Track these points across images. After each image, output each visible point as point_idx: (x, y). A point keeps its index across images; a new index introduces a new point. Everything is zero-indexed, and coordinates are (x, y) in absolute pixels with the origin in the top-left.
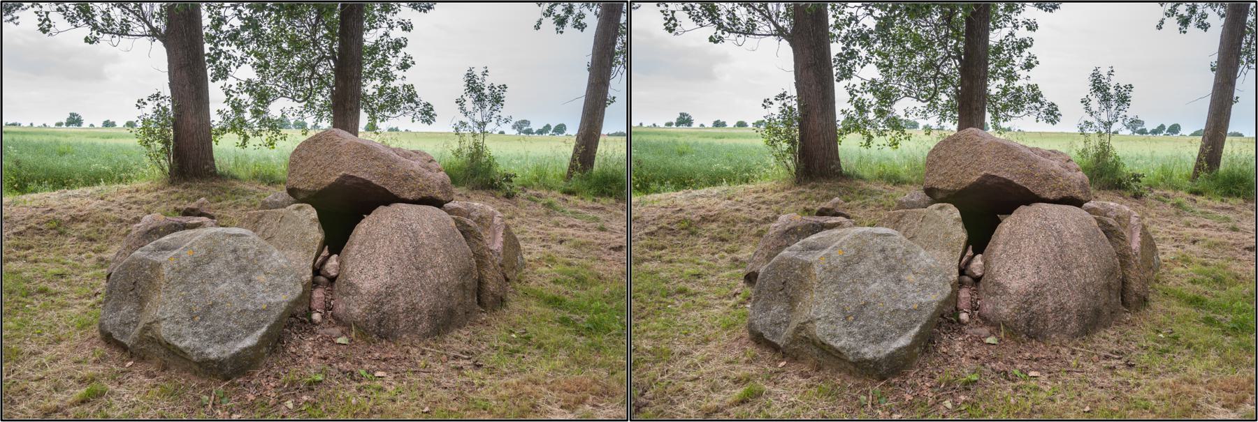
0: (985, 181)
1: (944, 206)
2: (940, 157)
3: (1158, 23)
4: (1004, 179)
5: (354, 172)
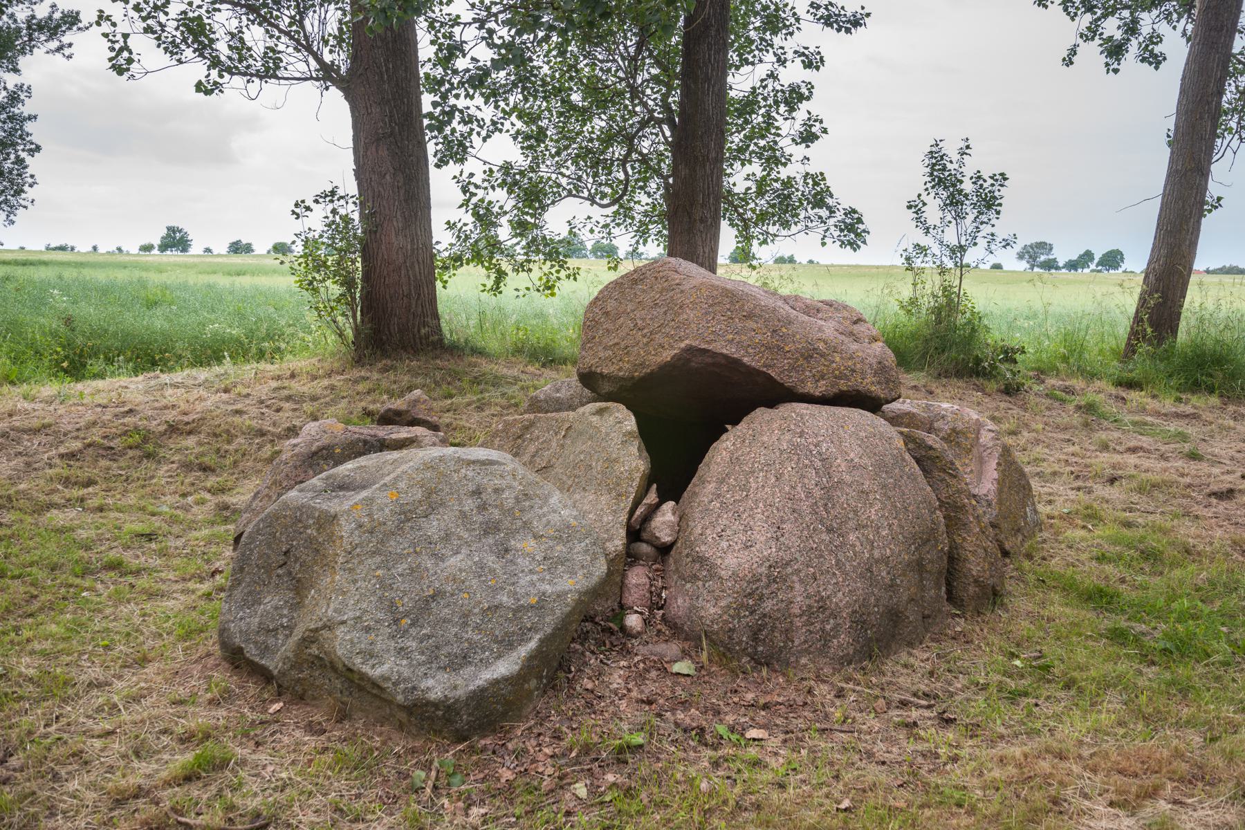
0: (689, 360)
1: (607, 408)
3: (1065, 54)
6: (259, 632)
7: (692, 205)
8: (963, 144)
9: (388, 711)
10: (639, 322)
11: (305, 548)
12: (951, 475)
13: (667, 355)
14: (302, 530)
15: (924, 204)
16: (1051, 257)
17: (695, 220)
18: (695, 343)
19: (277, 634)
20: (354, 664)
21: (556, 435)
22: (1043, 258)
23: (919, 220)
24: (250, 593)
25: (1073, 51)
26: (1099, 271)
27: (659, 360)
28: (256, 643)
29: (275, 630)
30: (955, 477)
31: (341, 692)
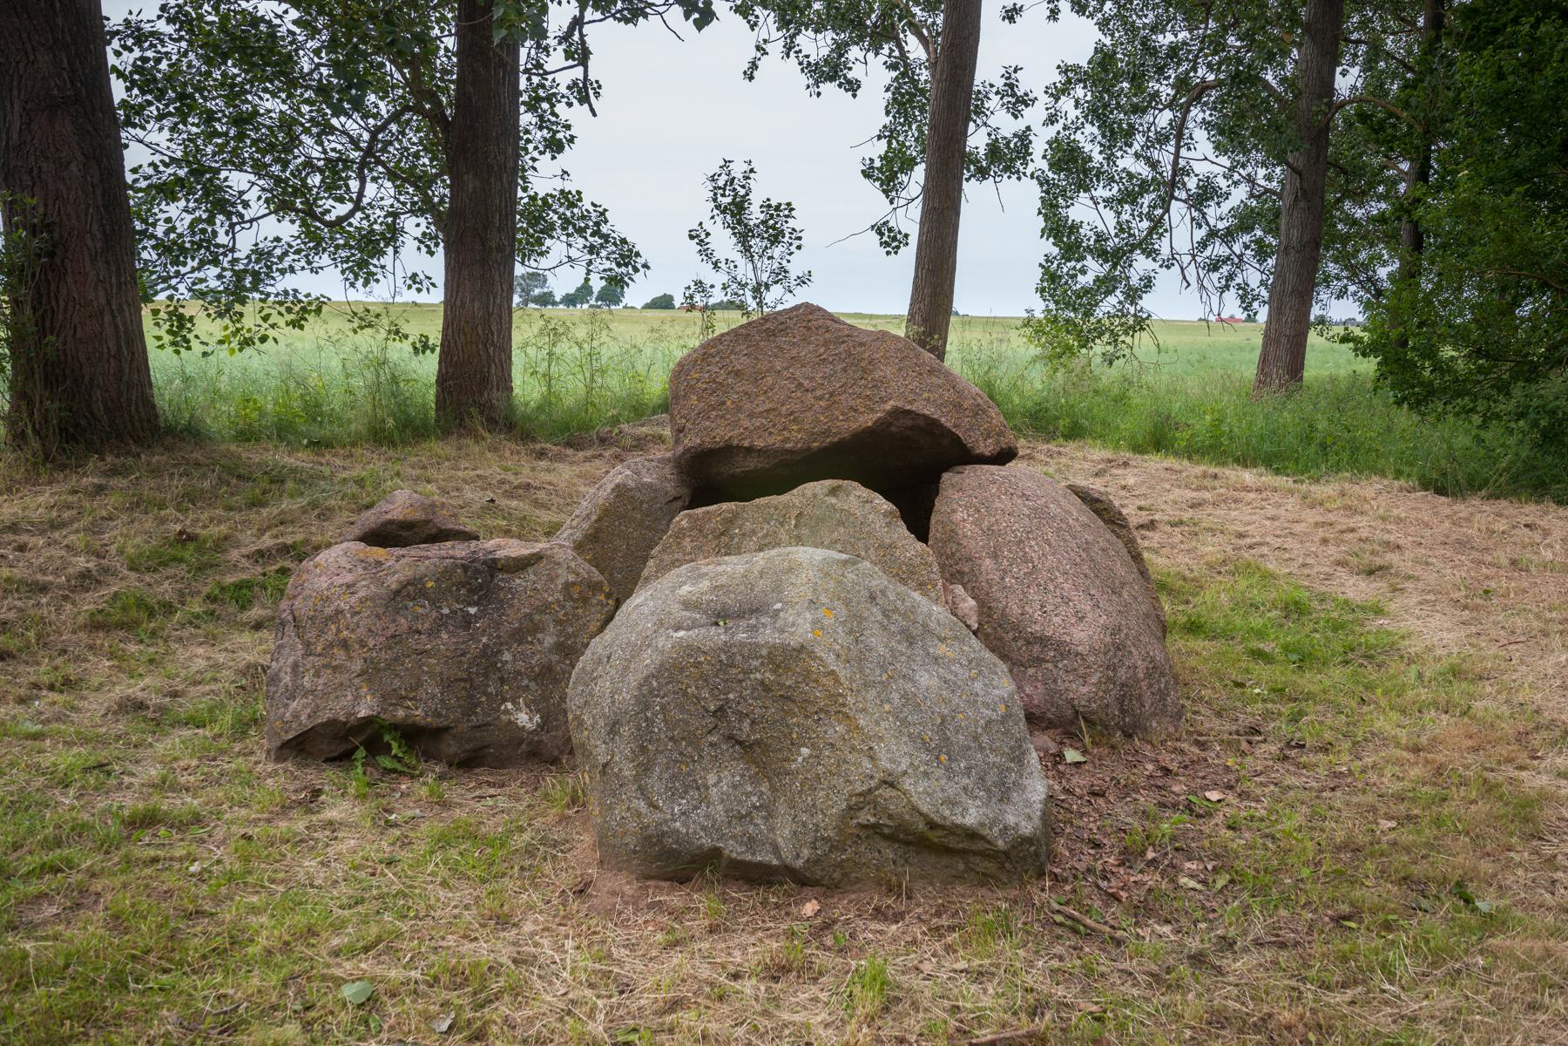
0: (890, 424)
1: (839, 487)
2: (737, 373)
3: (746, 66)
4: (925, 417)
5: (911, 402)
6: (729, 823)
7: (486, 229)
8: (746, 167)
9: (961, 867)
10: (806, 383)
11: (755, 699)
12: (1121, 526)
13: (868, 420)
14: (741, 676)
15: (708, 234)
16: (546, 290)
17: (491, 249)
18: (900, 404)
19: (751, 820)
20: (945, 818)
21: (782, 524)
22: (537, 291)
23: (706, 252)
24: (674, 777)
25: (754, 65)
26: (599, 307)
27: (854, 426)
28: (734, 837)
29: (749, 814)
30: (1124, 527)
31: (894, 863)
